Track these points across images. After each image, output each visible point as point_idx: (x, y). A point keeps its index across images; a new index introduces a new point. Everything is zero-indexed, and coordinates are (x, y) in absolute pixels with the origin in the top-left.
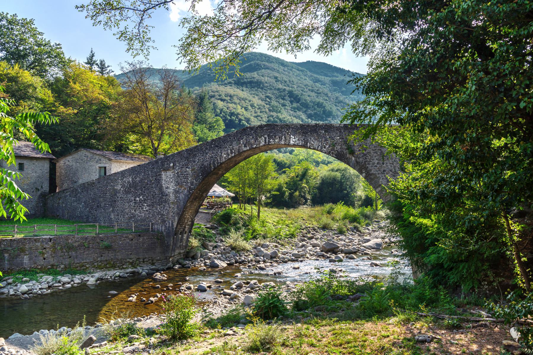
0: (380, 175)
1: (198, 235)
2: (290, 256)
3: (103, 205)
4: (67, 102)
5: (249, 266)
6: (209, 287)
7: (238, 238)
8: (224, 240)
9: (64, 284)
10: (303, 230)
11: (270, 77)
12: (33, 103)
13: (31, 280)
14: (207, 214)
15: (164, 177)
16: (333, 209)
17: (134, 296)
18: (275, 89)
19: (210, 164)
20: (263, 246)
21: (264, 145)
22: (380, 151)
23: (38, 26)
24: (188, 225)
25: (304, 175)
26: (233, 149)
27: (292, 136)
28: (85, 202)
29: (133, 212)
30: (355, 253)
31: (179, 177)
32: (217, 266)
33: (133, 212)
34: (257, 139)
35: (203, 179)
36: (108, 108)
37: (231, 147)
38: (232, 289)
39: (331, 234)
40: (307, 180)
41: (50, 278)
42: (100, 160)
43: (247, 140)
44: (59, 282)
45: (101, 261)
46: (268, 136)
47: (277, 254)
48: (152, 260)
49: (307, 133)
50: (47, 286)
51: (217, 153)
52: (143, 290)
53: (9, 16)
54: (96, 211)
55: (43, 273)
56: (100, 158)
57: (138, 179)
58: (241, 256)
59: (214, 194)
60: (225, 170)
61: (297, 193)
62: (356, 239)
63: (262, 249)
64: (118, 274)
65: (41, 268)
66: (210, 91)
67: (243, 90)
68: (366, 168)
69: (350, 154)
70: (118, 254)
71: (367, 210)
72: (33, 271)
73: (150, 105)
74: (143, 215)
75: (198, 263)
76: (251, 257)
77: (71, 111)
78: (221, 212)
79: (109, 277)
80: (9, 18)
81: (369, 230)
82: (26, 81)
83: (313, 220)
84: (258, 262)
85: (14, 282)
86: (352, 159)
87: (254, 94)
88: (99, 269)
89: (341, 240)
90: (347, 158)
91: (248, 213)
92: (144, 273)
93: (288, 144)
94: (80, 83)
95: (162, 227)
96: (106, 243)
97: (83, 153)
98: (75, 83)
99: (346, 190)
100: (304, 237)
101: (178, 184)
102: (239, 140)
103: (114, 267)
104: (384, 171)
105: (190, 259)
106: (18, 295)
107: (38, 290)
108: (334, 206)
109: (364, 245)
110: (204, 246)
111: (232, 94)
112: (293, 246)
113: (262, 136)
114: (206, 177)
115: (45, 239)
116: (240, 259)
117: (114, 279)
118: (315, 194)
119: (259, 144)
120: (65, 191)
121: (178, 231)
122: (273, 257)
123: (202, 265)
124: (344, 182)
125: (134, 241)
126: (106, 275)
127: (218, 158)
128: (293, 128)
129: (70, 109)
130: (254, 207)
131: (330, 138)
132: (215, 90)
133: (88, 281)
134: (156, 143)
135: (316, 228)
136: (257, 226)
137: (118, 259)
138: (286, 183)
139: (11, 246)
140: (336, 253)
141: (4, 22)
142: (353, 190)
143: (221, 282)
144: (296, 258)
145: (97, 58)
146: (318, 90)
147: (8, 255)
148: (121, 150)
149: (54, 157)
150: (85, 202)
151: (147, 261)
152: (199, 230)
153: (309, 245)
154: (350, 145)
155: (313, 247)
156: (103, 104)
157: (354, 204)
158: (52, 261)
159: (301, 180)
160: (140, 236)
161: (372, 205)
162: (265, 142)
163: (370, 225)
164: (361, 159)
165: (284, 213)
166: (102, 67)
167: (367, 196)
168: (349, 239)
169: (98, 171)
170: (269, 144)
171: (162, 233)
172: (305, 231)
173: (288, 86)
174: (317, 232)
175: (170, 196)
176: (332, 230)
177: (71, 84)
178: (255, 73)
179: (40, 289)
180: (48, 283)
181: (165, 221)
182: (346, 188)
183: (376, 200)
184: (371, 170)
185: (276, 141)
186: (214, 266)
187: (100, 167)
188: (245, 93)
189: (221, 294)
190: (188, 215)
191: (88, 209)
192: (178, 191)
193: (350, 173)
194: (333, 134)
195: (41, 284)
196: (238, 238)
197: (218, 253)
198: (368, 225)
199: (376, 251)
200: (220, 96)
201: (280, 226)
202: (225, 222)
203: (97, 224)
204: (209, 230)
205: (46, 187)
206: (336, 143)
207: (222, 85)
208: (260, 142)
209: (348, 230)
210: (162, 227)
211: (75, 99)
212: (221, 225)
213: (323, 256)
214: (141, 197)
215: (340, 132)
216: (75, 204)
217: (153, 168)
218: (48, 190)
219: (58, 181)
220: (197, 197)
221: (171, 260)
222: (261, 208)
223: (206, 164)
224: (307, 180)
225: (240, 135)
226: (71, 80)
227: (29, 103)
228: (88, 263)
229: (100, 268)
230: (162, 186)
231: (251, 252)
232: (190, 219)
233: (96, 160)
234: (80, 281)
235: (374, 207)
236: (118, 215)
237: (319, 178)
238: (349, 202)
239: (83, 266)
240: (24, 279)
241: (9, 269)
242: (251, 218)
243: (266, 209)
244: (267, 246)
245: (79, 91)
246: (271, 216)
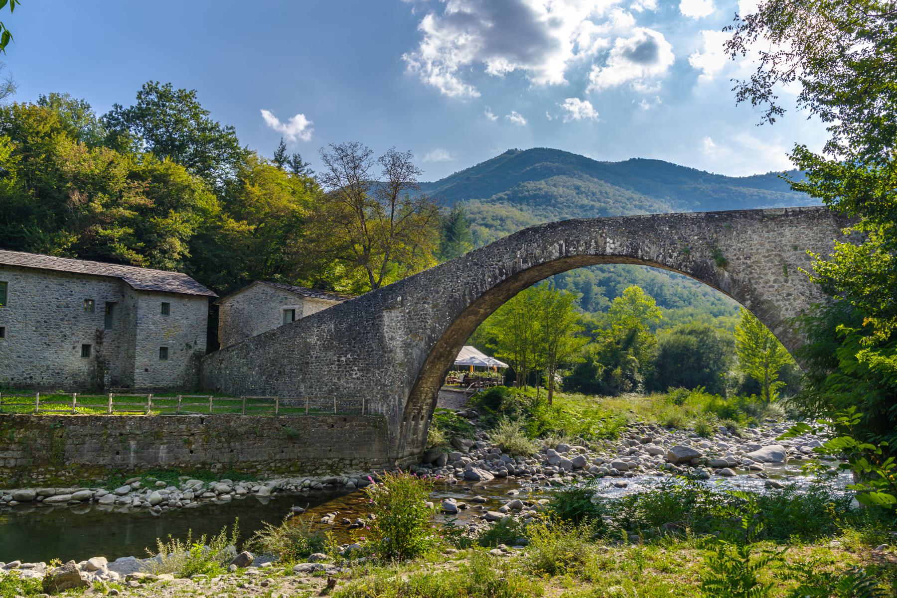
0: (781, 303)
1: (443, 425)
2: (609, 467)
3: (287, 369)
4: (241, 214)
5: (534, 480)
6: (462, 507)
7: (513, 432)
8: (488, 436)
9: (220, 494)
10: (631, 427)
11: (568, 188)
12: (190, 215)
13: (169, 484)
14: (461, 395)
16: (686, 397)
17: (331, 515)
18: (576, 206)
19: (464, 295)
21: (558, 259)
24: (427, 404)
25: (631, 340)
26: (504, 267)
27: (608, 240)
29: (336, 380)
30: (732, 467)
32: (477, 479)
33: (336, 380)
34: (546, 248)
35: (453, 322)
36: (303, 222)
37: (501, 263)
38: (504, 512)
39: (683, 436)
40: (636, 349)
41: (198, 484)
42: (286, 298)
43: (527, 251)
44: (213, 491)
45: (281, 461)
46: (566, 241)
48: (366, 463)
49: (636, 232)
51: (476, 275)
52: (347, 507)
53: (160, 87)
54: (277, 380)
55: (188, 475)
56: (286, 294)
57: (344, 325)
59: (472, 363)
61: (618, 371)
62: (733, 446)
63: (558, 454)
64: (308, 482)
65: (186, 467)
66: (468, 212)
67: (521, 210)
69: (719, 265)
71: (752, 402)
73: (368, 211)
74: (352, 385)
75: (444, 472)
76: (537, 466)
78: (484, 392)
79: (293, 487)
81: (755, 433)
82: (179, 180)
83: (650, 414)
84: (551, 474)
85: (142, 487)
87: (540, 215)
88: (278, 473)
90: (714, 274)
92: (350, 483)
94: (260, 185)
95: (382, 406)
96: (291, 429)
97: (260, 288)
98: (253, 186)
99: (707, 366)
100: (633, 438)
101: (410, 331)
102: (513, 252)
103: (301, 471)
105: (430, 465)
106: (145, 507)
107: (178, 500)
108: (688, 392)
109: (750, 454)
110: (455, 445)
112: (613, 452)
113: (554, 242)
114: (457, 317)
115: (194, 418)
116: (516, 468)
117: (302, 491)
120: (230, 349)
121: (410, 413)
123: (451, 476)
124: (704, 353)
125: (335, 429)
126: (288, 484)
129: (243, 224)
130: (542, 389)
131: (679, 238)
132: (476, 210)
133: (258, 491)
134: (377, 278)
135: (655, 426)
138: (599, 353)
141: (153, 97)
142: (722, 366)
143: (482, 502)
144: (621, 471)
145: (289, 153)
146: (650, 206)
149: (215, 295)
152: (445, 418)
153: (642, 451)
154: (720, 251)
155: (652, 455)
157: (725, 393)
158: (202, 456)
159: (625, 348)
161: (758, 394)
162: (561, 253)
166: (297, 165)
167: (749, 378)
170: (567, 256)
171: (382, 416)
172: (634, 430)
173: (599, 201)
174: (657, 432)
175: (395, 354)
176: (685, 430)
178: (543, 182)
179: (181, 499)
180: (195, 490)
181: (388, 396)
182: (708, 364)
183: (767, 385)
185: (580, 249)
186: (471, 478)
187: (286, 311)
188: (525, 214)
189: (482, 518)
190: (427, 387)
192: (410, 344)
193: (715, 338)
194: (685, 232)
195: (183, 493)
196: (513, 432)
197: (479, 458)
198: (752, 425)
199: (774, 466)
200: (483, 219)
203: (276, 398)
204: (462, 419)
205: (202, 344)
206: (692, 248)
207: (487, 202)
209: (715, 431)
210: (382, 406)
212: (484, 412)
213: (671, 470)
214: (349, 356)
215: (700, 227)
216: (246, 368)
217: (369, 306)
218: (205, 348)
219: (220, 334)
220: (441, 355)
221: (396, 463)
223: (456, 295)
224: (636, 349)
225: (515, 243)
226: (247, 181)
227: (183, 214)
229: (278, 472)
230: (383, 336)
231: (538, 458)
234: (245, 491)
235: (764, 398)
236: (311, 387)
237: (657, 345)
239: (252, 467)
240: (159, 482)
241: (136, 466)
242: (536, 403)
244: (567, 449)
245: (259, 197)
246: (574, 406)
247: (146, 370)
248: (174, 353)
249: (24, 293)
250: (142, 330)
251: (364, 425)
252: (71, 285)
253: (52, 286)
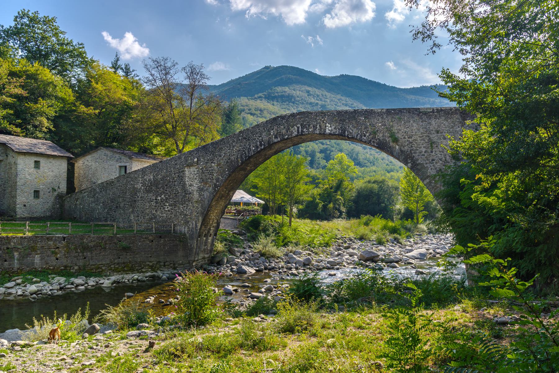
2: (325, 264)
5: (280, 273)
6: (236, 291)
7: (267, 243)
9: (77, 286)
10: (339, 239)
11: (302, 91)
12: (53, 102)
14: (235, 221)
15: (187, 173)
16: (371, 221)
18: (307, 103)
20: (295, 253)
21: (297, 136)
22: (428, 138)
23: (60, 24)
24: (213, 227)
25: (339, 186)
27: (327, 125)
28: (103, 203)
29: (154, 212)
31: (204, 173)
32: (245, 272)
33: (154, 212)
34: (289, 129)
35: (230, 175)
36: (132, 108)
37: (261, 138)
38: (261, 292)
41: (62, 280)
42: (121, 159)
43: (277, 131)
44: (72, 284)
45: (118, 264)
46: (301, 125)
47: (311, 262)
48: (174, 264)
49: (344, 120)
50: (58, 287)
52: (162, 292)
54: (115, 212)
56: (121, 156)
57: (160, 176)
58: (270, 262)
60: (254, 166)
61: (331, 205)
62: (397, 250)
63: (295, 256)
64: (136, 277)
65: (53, 269)
66: (240, 105)
67: (273, 105)
68: (412, 158)
69: (393, 142)
71: (408, 223)
72: (44, 272)
75: (224, 268)
77: (91, 111)
78: (250, 218)
79: (126, 281)
80: (31, 15)
81: (410, 242)
82: (45, 78)
84: (290, 269)
85: (23, 282)
86: (395, 147)
87: (285, 108)
88: (116, 272)
89: (381, 250)
90: (390, 147)
91: (279, 221)
92: (164, 277)
93: (324, 134)
95: (185, 228)
96: (124, 244)
98: (97, 83)
99: (383, 202)
101: (202, 181)
102: (269, 131)
103: (132, 270)
104: (433, 160)
109: (407, 254)
111: (263, 108)
112: (328, 255)
113: (294, 125)
114: (232, 172)
115: (58, 237)
116: (269, 265)
117: (132, 282)
118: (351, 207)
119: (291, 135)
120: (83, 192)
122: (306, 264)
124: (381, 194)
126: (123, 278)
127: (246, 151)
128: (329, 116)
129: (91, 109)
130: (285, 217)
131: (370, 125)
132: (245, 104)
133: (103, 284)
135: (353, 238)
136: (289, 233)
138: (320, 195)
139: (21, 244)
140: (376, 262)
141: (25, 20)
143: (248, 287)
144: (332, 266)
145: (121, 63)
146: (352, 104)
147: (18, 253)
148: (145, 152)
150: (103, 203)
151: (168, 265)
155: (350, 256)
156: (126, 105)
157: (393, 218)
158: (64, 261)
159: (336, 192)
160: (160, 237)
162: (298, 132)
163: (411, 237)
164: (406, 148)
165: (318, 224)
167: (407, 210)
168: (390, 250)
169: (118, 170)
170: (302, 135)
171: (185, 234)
172: (340, 241)
174: (354, 242)
177: (93, 84)
179: (51, 290)
180: (60, 284)
181: (188, 222)
182: (384, 201)
184: (417, 160)
185: (310, 130)
186: (241, 272)
187: (120, 167)
189: (248, 297)
190: (213, 216)
191: (106, 210)
192: (202, 189)
196: (267, 243)
197: (246, 260)
198: (408, 237)
199: (421, 261)
200: (249, 110)
201: (313, 235)
202: (253, 228)
203: (114, 224)
205: (63, 187)
206: (377, 131)
208: (292, 132)
209: (387, 241)
210: (185, 228)
211: (97, 99)
212: (250, 231)
213: (362, 265)
214: (163, 196)
215: (382, 118)
216: (94, 204)
217: (176, 164)
220: (223, 196)
221: (194, 264)
222: (293, 219)
223: (232, 158)
224: (342, 192)
225: (270, 125)
226: (93, 80)
227: (49, 101)
228: (104, 265)
230: (185, 184)
231: (282, 259)
232: (215, 221)
233: (116, 159)
234: (94, 284)
235: (415, 221)
236: (138, 216)
237: (354, 190)
238: (386, 214)
239: (99, 268)
240: (35, 279)
241: (18, 269)
242: (282, 225)
243: (298, 220)
244: (300, 253)
246: (305, 226)
247: (25, 206)
248: (44, 194)
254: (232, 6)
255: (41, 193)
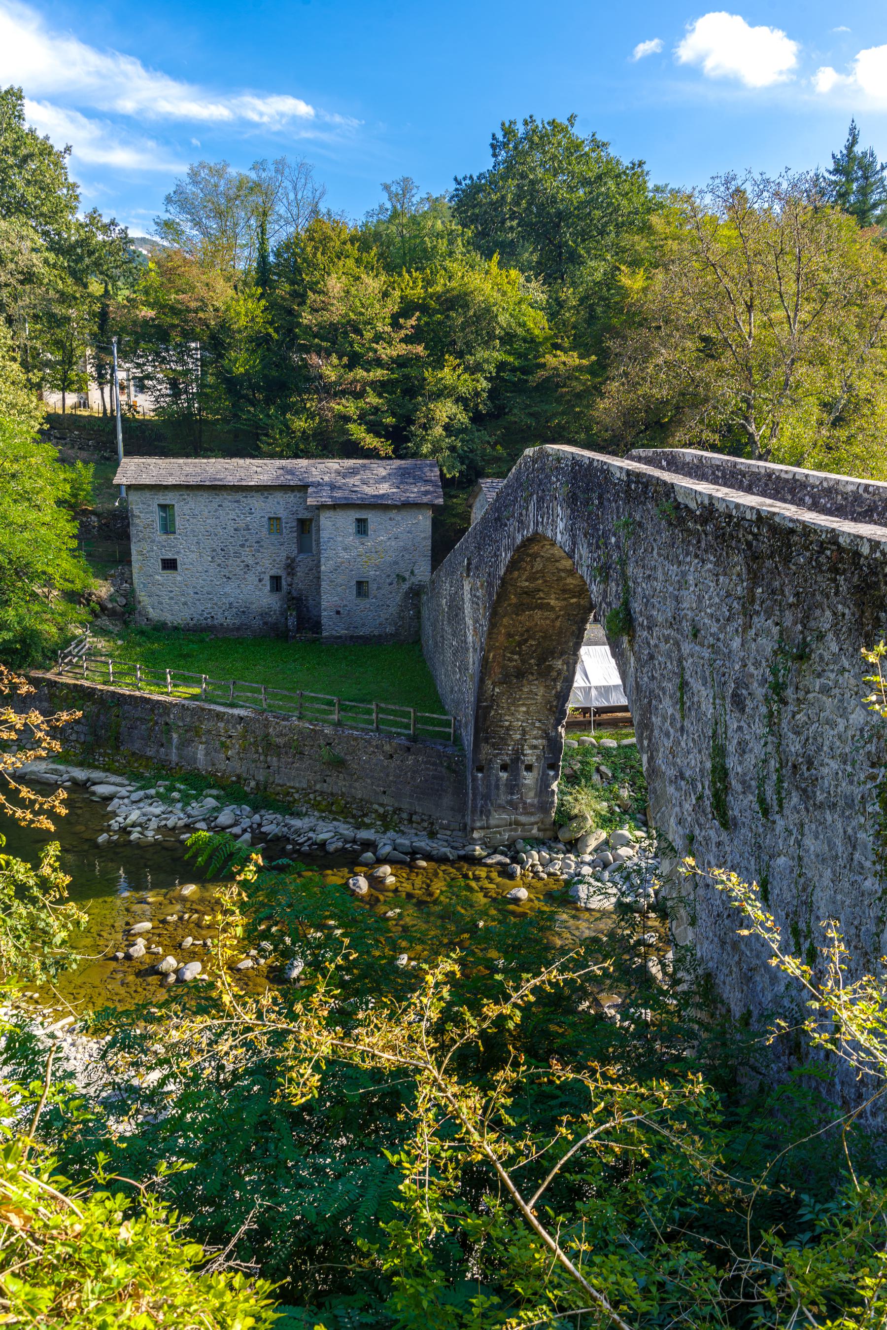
45: (322, 793)
70: (357, 784)
137: (354, 798)
158: (238, 767)
247: (338, 613)
248: (379, 588)
249: (194, 516)
250: (328, 559)
251: (434, 764)
252: (250, 501)
253: (226, 504)
254: (679, 58)
255: (373, 586)
